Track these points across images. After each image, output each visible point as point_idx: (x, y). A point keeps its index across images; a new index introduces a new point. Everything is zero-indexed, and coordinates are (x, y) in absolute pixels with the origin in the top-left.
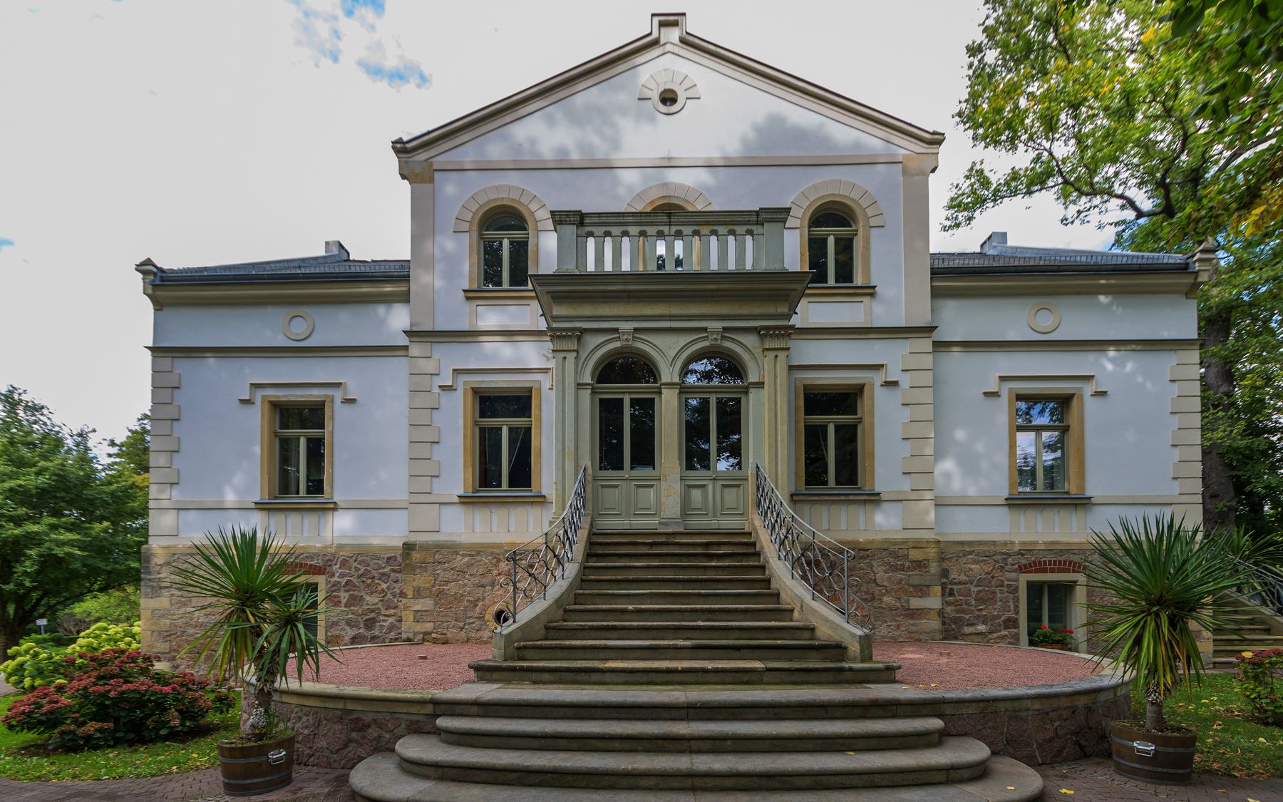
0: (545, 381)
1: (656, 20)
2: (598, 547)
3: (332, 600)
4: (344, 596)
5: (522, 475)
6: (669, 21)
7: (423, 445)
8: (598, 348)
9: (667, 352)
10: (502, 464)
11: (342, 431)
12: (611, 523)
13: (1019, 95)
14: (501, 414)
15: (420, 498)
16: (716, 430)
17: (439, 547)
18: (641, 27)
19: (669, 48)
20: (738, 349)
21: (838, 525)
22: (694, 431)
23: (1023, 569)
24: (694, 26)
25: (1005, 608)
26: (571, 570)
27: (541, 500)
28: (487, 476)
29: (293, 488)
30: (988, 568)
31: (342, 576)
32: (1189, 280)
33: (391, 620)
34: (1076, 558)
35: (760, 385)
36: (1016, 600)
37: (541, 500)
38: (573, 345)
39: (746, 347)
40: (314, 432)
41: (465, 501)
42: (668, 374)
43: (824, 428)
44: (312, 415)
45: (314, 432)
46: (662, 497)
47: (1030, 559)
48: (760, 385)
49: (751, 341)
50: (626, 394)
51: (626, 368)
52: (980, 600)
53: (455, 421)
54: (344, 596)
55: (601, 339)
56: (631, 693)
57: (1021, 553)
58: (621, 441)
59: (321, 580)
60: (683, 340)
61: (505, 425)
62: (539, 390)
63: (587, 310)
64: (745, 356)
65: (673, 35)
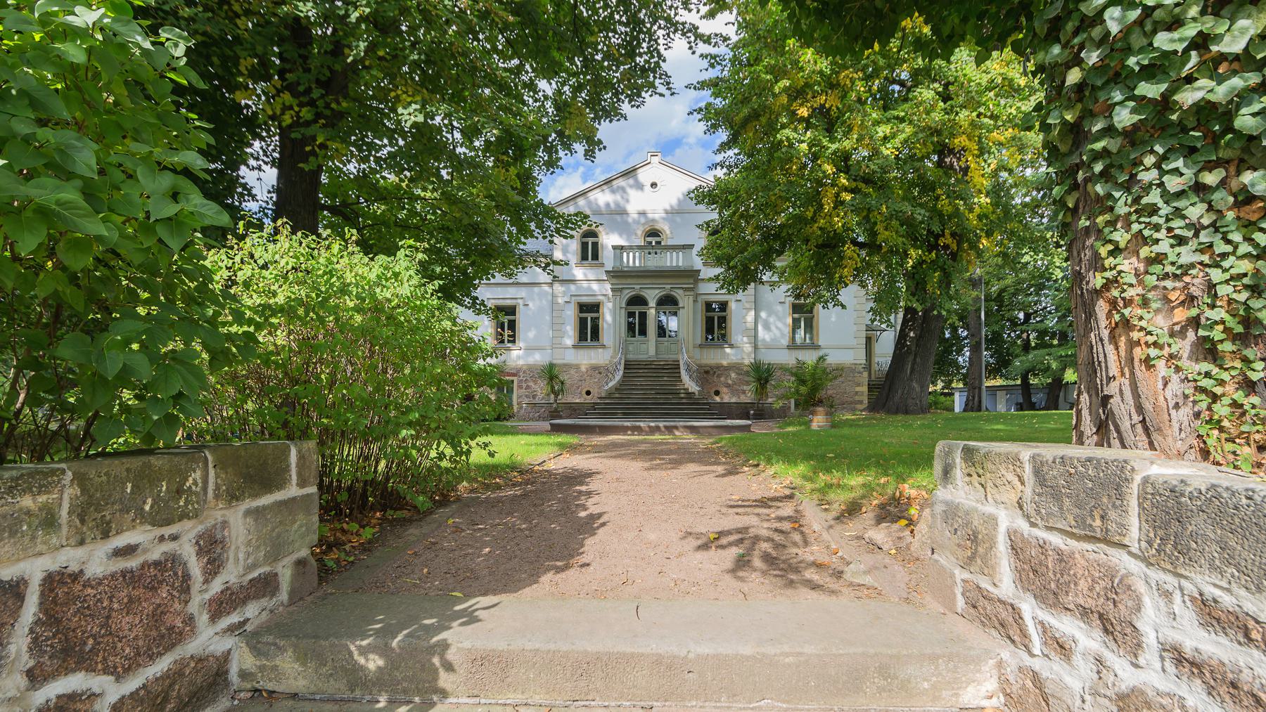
2: (628, 365)
4: (524, 385)
5: (596, 334)
7: (556, 325)
8: (628, 294)
9: (652, 296)
10: (589, 331)
11: (521, 319)
12: (631, 357)
13: (1080, 378)
14: (588, 315)
15: (556, 345)
17: (565, 365)
21: (712, 357)
26: (621, 373)
27: (603, 346)
28: (582, 336)
32: (224, 219)
37: (603, 346)
39: (678, 294)
40: (512, 318)
41: (574, 347)
44: (511, 311)
45: (594, 315)
46: (648, 348)
49: (680, 292)
50: (637, 310)
51: (638, 300)
53: (571, 314)
54: (524, 385)
56: (595, 461)
58: (636, 326)
59: (515, 379)
61: (589, 316)
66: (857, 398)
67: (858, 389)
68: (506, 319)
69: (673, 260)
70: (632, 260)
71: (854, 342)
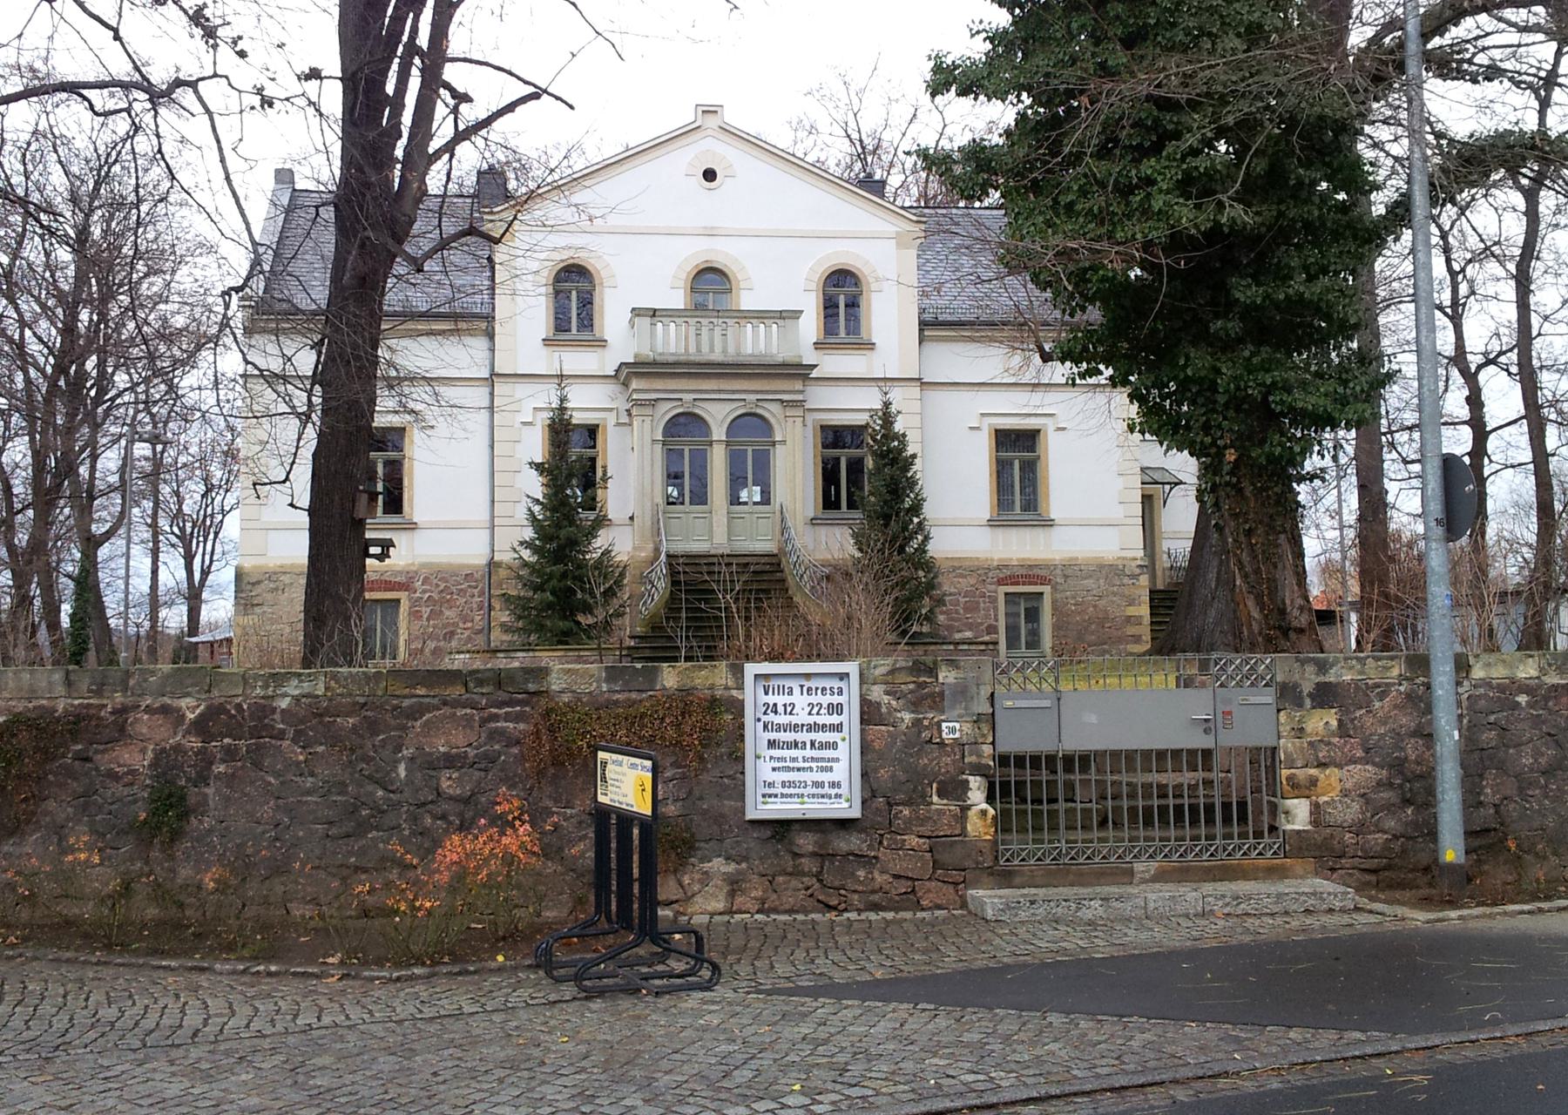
0: (611, 419)
1: (700, 109)
3: (415, 615)
6: (710, 111)
8: (666, 411)
9: (718, 416)
16: (751, 467)
18: (686, 116)
19: (709, 132)
20: (767, 415)
22: (736, 481)
23: (1001, 582)
24: (732, 117)
25: (987, 616)
29: (774, 561)
30: (973, 581)
31: (424, 592)
33: (467, 633)
34: (1042, 573)
35: (784, 442)
36: (996, 609)
38: (649, 411)
39: (772, 412)
42: (719, 433)
43: (838, 460)
47: (1009, 575)
48: (784, 442)
49: (775, 408)
51: (685, 426)
52: (966, 609)
54: (426, 611)
55: (670, 405)
57: (998, 568)
59: (403, 595)
60: (729, 407)
62: (605, 427)
63: (659, 384)
64: (772, 420)
65: (712, 122)
66: (1131, 630)
67: (1131, 611)
68: (1016, 457)
69: (755, 342)
70: (671, 341)
71: (1117, 513)
